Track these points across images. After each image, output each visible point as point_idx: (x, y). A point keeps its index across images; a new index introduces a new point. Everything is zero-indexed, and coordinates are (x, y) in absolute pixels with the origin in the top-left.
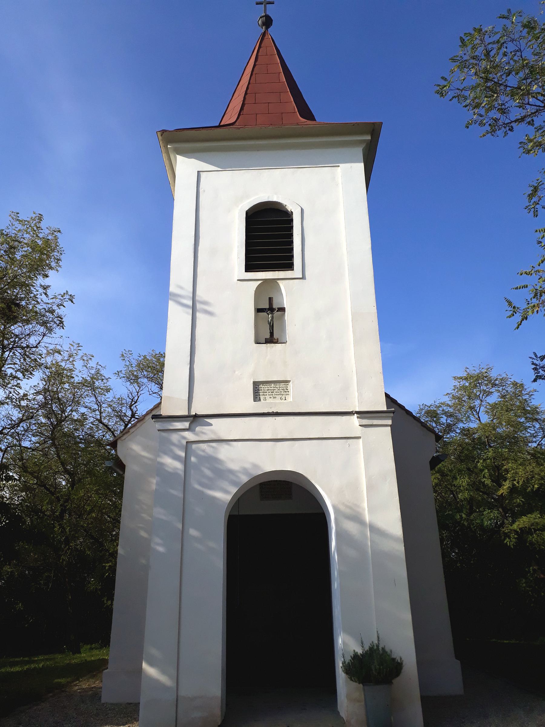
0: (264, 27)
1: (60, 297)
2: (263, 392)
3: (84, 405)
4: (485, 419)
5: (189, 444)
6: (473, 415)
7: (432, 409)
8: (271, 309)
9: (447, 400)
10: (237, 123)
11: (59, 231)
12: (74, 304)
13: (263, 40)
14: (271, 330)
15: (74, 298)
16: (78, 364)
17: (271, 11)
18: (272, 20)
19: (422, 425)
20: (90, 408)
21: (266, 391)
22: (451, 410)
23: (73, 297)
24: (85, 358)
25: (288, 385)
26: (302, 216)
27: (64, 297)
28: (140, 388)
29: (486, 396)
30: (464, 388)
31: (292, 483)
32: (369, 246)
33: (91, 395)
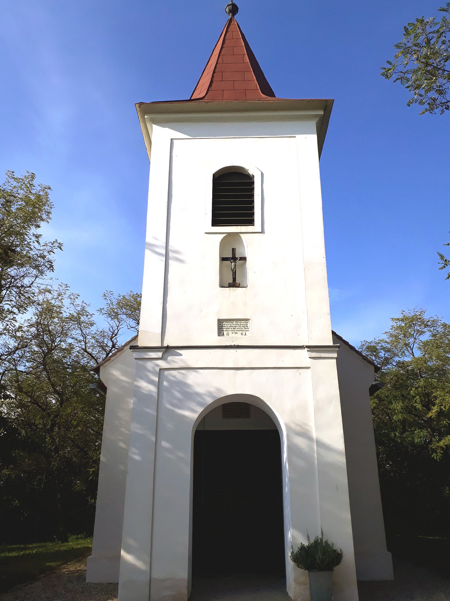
1: (50, 245)
2: (226, 328)
3: (71, 336)
4: (418, 354)
5: (162, 371)
6: (408, 350)
7: (372, 345)
8: (234, 258)
9: (385, 337)
10: (206, 98)
11: (50, 188)
12: (62, 250)
14: (234, 276)
16: (66, 302)
19: (363, 358)
20: (76, 340)
21: (229, 327)
23: (62, 245)
24: (72, 297)
27: (54, 245)
28: (120, 323)
30: (400, 328)
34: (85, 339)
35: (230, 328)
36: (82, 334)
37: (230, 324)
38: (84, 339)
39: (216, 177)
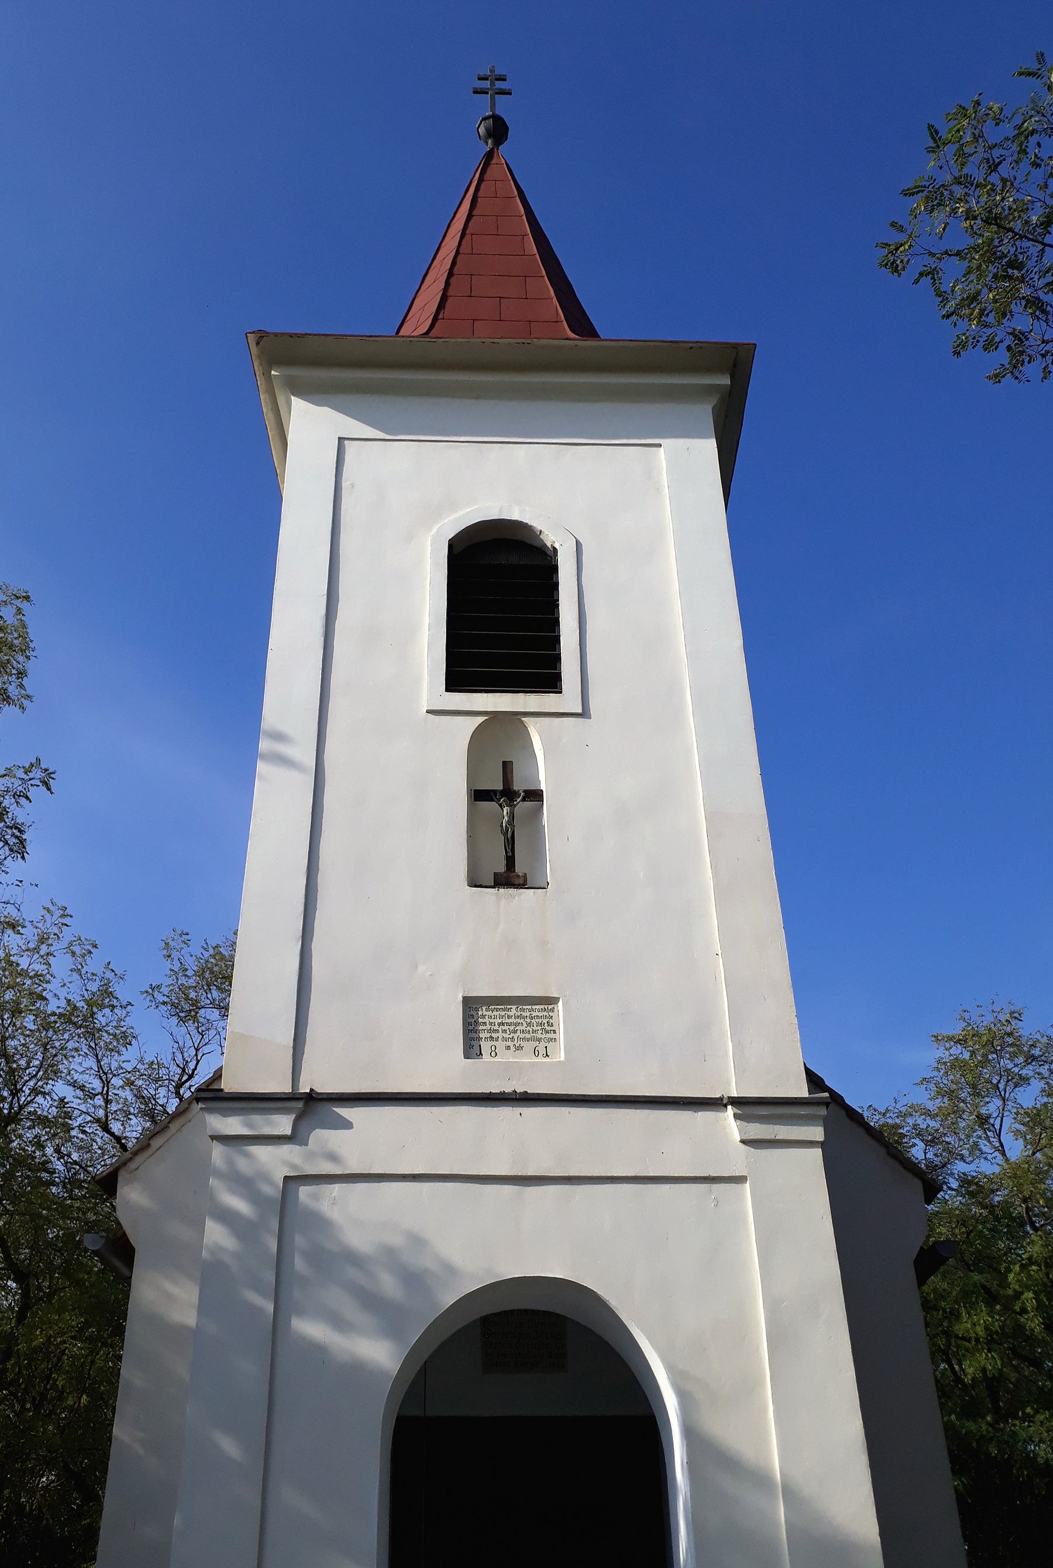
0: (490, 141)
1: (20, 774)
2: (490, 1031)
3: (68, 1077)
4: (1016, 1149)
5: (292, 1185)
6: (987, 1138)
7: (890, 1121)
8: (508, 794)
9: (923, 1097)
11: (27, 598)
12: (52, 793)
13: (488, 167)
14: (509, 851)
15: (52, 778)
16: (61, 964)
17: (504, 108)
18: (507, 128)
19: (888, 1153)
20: (82, 1088)
21: (496, 1027)
22: (934, 1124)
23: (52, 775)
24: (77, 949)
25: (552, 1010)
26: (579, 549)
27: (31, 775)
28: (203, 1036)
29: (1015, 1087)
30: (956, 1064)
31: (566, 1317)
32: (738, 642)
33: (87, 1051)
34: (106, 1089)
35: (500, 1031)
36: (99, 1072)
37: (502, 1017)
38: (103, 1087)
39: (455, 552)
